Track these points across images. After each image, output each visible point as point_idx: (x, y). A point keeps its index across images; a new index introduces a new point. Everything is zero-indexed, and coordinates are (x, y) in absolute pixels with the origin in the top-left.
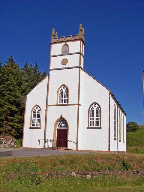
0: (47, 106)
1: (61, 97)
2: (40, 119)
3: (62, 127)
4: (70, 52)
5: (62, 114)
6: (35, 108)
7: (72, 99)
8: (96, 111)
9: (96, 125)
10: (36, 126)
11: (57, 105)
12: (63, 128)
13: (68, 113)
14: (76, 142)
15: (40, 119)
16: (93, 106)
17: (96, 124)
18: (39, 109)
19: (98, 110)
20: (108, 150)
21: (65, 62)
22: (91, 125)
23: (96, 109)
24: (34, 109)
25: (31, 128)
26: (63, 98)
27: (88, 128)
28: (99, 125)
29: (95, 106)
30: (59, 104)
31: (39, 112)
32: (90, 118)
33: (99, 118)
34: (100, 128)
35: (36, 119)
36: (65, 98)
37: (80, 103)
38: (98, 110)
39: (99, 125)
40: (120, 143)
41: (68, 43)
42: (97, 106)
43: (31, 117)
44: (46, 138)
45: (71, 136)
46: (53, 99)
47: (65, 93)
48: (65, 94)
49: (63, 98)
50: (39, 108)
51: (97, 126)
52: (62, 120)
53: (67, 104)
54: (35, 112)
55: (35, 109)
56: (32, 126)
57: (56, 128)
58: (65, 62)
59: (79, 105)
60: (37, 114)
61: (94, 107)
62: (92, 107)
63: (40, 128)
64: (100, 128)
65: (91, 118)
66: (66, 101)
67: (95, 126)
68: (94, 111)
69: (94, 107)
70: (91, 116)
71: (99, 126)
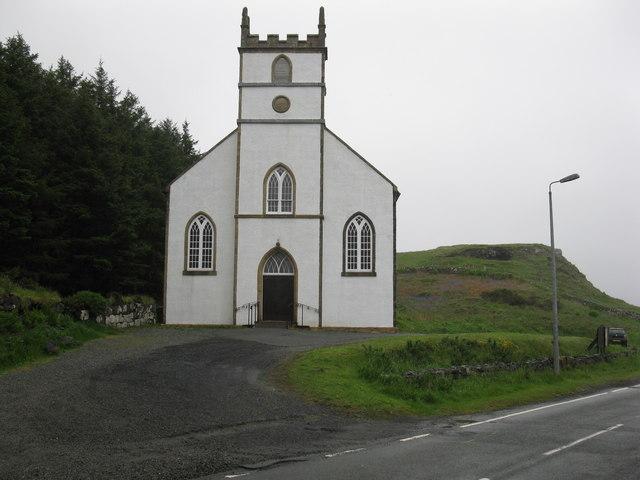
0: (237, 217)
6: (197, 221)
7: (306, 203)
10: (200, 268)
13: (297, 239)
16: (354, 221)
21: (281, 104)
25: (186, 273)
26: (280, 199)
27: (344, 274)
29: (359, 223)
30: (268, 213)
34: (373, 274)
42: (364, 221)
43: (186, 243)
45: (305, 294)
46: (253, 200)
49: (280, 199)
51: (364, 270)
52: (278, 254)
56: (189, 269)
58: (281, 104)
60: (202, 237)
62: (353, 224)
63: (214, 273)
64: (373, 274)
66: (288, 204)
67: (359, 269)
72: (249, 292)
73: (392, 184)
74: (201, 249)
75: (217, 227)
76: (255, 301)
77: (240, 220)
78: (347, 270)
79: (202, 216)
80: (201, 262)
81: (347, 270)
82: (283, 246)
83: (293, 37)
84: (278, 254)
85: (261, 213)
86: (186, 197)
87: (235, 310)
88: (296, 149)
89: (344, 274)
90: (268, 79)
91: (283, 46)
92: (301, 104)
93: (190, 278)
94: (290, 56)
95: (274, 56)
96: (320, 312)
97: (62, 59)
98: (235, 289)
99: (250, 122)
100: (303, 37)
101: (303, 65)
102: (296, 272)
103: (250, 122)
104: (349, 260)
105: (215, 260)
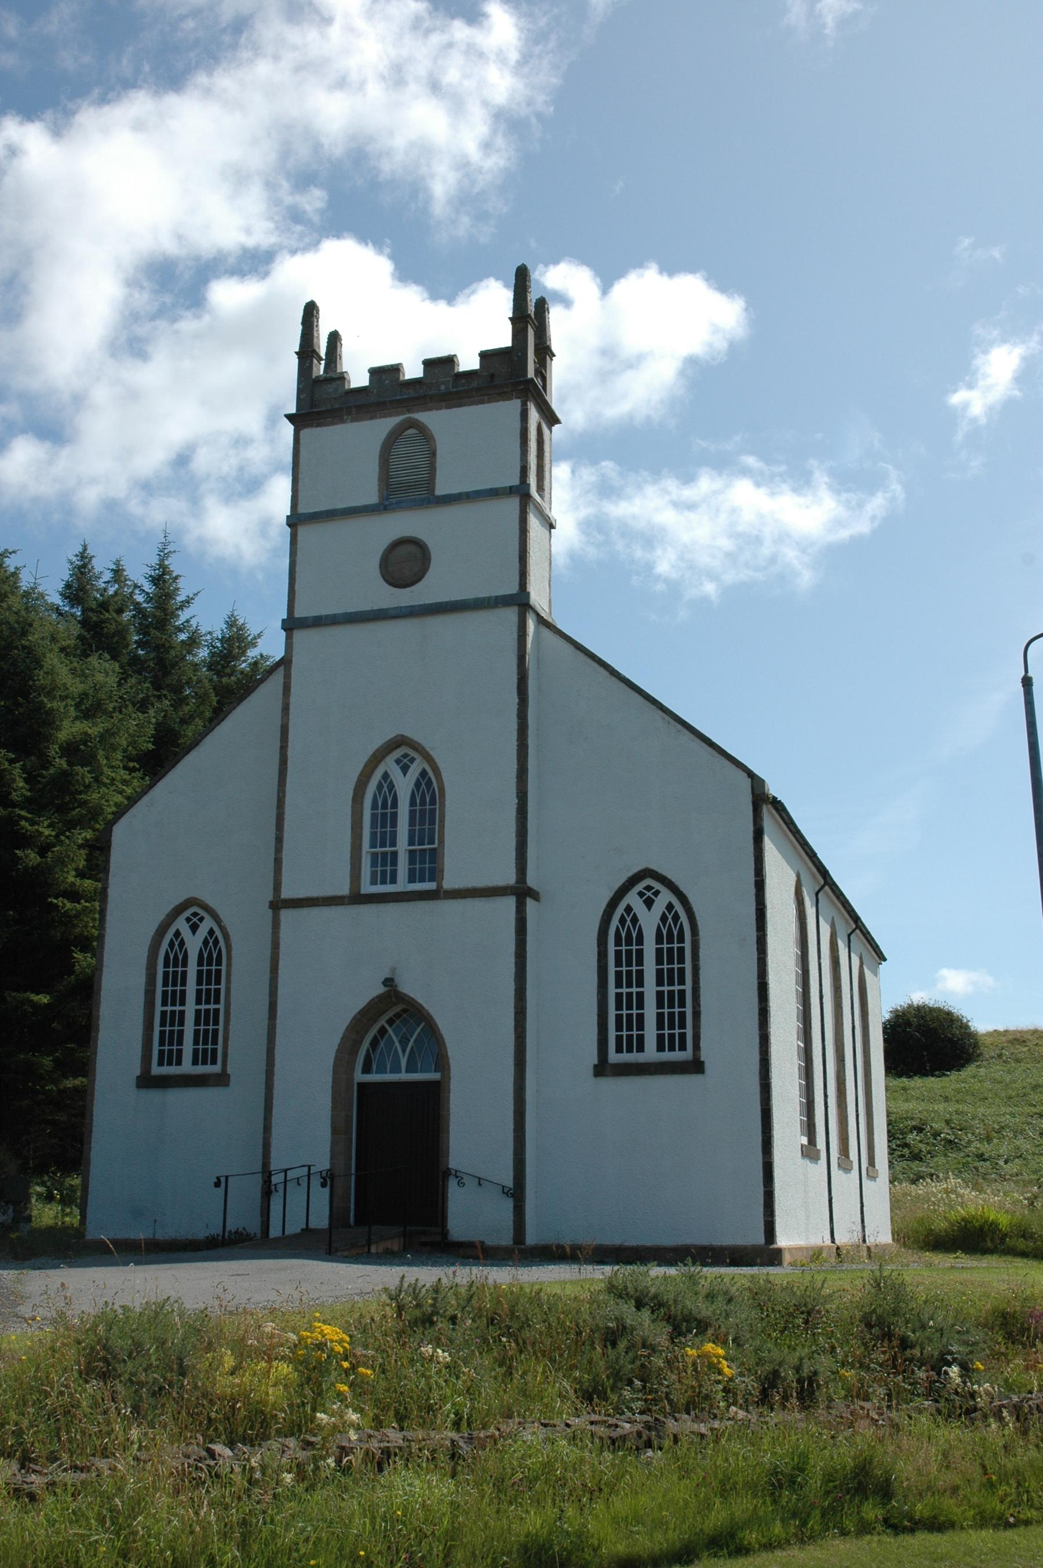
0: (278, 905)
1: (384, 834)
2: (221, 1006)
3: (396, 1069)
4: (440, 490)
5: (393, 970)
6: (181, 924)
7: (476, 849)
8: (659, 939)
9: (660, 1048)
10: (187, 1067)
11: (357, 898)
12: (404, 1076)
13: (448, 960)
14: (509, 1183)
15: (221, 1006)
16: (632, 898)
17: (660, 1038)
18: (211, 932)
19: (176, 957)
20: (761, 1240)
21: (405, 563)
22: (619, 1050)
23: (412, 786)
24: (169, 935)
25: (147, 1081)
26: (402, 845)
27: (602, 1068)
28: (683, 1047)
29: (649, 903)
30: (367, 888)
31: (214, 956)
32: (612, 990)
33: (682, 993)
34: (696, 1066)
35: (190, 1008)
36: (411, 842)
37: (531, 881)
38: (176, 957)
39: (683, 1047)
40: (845, 1183)
41: (424, 417)
42: (665, 897)
43: (150, 993)
44: (276, 1163)
45: (474, 1135)
46: (321, 857)
47: (413, 803)
48: (412, 813)
49: (402, 845)
50: (207, 924)
51: (667, 1056)
52: (395, 1014)
53: (431, 886)
54: (177, 958)
55: (177, 934)
56: (156, 1070)
57: (353, 1079)
58: (405, 563)
59: (522, 892)
60: (193, 974)
61: (396, 773)
62: (629, 909)
63: (222, 1080)
64: (696, 1066)
65: (618, 996)
66: (428, 862)
67: (650, 1053)
68: (185, 964)
69: (396, 773)
70: (619, 974)
71: (687, 1055)
72: (308, 1131)
73: (751, 774)
74: (650, 988)
75: (234, 939)
76: (323, 1163)
77: (285, 915)
78: (613, 1057)
79: (193, 909)
80: (190, 1044)
81: (613, 1057)
82: (408, 987)
83: (440, 366)
84: (395, 1014)
85: (345, 890)
86: (165, 854)
87: (267, 1191)
88: (439, 689)
89: (602, 1068)
90: (370, 495)
91: (411, 393)
92: (459, 551)
93: (154, 1096)
94: (433, 419)
95: (382, 427)
96: (517, 1193)
97: (83, 555)
98: (267, 1128)
99: (318, 622)
100: (469, 362)
101: (466, 442)
102: (442, 1063)
103: (318, 622)
104: (163, 1036)
105: (226, 1040)
